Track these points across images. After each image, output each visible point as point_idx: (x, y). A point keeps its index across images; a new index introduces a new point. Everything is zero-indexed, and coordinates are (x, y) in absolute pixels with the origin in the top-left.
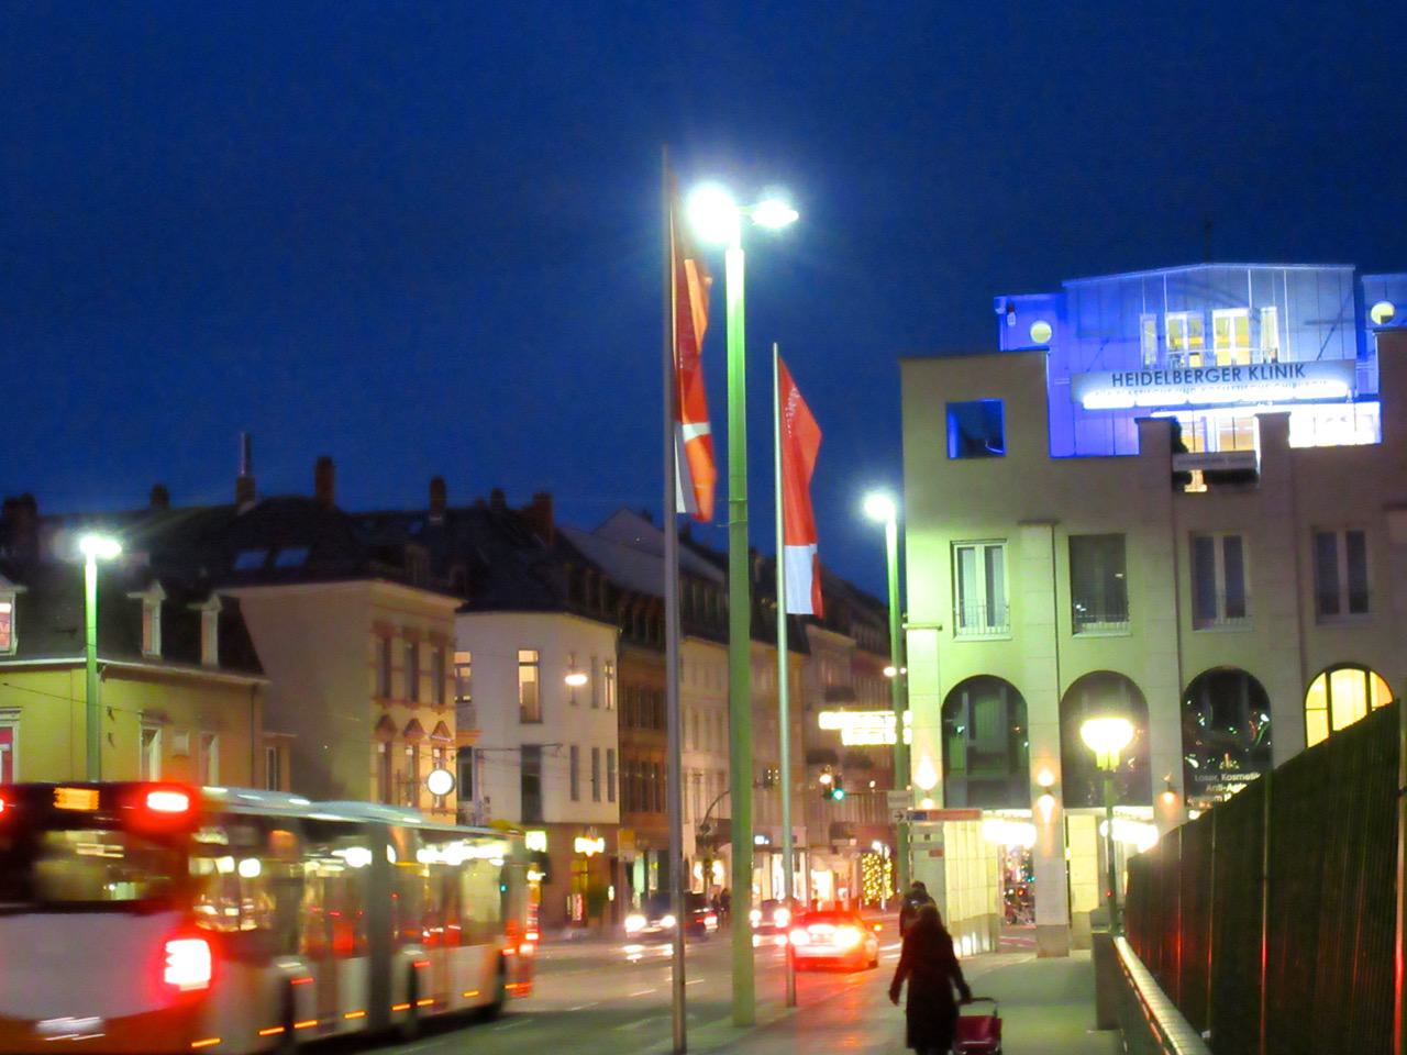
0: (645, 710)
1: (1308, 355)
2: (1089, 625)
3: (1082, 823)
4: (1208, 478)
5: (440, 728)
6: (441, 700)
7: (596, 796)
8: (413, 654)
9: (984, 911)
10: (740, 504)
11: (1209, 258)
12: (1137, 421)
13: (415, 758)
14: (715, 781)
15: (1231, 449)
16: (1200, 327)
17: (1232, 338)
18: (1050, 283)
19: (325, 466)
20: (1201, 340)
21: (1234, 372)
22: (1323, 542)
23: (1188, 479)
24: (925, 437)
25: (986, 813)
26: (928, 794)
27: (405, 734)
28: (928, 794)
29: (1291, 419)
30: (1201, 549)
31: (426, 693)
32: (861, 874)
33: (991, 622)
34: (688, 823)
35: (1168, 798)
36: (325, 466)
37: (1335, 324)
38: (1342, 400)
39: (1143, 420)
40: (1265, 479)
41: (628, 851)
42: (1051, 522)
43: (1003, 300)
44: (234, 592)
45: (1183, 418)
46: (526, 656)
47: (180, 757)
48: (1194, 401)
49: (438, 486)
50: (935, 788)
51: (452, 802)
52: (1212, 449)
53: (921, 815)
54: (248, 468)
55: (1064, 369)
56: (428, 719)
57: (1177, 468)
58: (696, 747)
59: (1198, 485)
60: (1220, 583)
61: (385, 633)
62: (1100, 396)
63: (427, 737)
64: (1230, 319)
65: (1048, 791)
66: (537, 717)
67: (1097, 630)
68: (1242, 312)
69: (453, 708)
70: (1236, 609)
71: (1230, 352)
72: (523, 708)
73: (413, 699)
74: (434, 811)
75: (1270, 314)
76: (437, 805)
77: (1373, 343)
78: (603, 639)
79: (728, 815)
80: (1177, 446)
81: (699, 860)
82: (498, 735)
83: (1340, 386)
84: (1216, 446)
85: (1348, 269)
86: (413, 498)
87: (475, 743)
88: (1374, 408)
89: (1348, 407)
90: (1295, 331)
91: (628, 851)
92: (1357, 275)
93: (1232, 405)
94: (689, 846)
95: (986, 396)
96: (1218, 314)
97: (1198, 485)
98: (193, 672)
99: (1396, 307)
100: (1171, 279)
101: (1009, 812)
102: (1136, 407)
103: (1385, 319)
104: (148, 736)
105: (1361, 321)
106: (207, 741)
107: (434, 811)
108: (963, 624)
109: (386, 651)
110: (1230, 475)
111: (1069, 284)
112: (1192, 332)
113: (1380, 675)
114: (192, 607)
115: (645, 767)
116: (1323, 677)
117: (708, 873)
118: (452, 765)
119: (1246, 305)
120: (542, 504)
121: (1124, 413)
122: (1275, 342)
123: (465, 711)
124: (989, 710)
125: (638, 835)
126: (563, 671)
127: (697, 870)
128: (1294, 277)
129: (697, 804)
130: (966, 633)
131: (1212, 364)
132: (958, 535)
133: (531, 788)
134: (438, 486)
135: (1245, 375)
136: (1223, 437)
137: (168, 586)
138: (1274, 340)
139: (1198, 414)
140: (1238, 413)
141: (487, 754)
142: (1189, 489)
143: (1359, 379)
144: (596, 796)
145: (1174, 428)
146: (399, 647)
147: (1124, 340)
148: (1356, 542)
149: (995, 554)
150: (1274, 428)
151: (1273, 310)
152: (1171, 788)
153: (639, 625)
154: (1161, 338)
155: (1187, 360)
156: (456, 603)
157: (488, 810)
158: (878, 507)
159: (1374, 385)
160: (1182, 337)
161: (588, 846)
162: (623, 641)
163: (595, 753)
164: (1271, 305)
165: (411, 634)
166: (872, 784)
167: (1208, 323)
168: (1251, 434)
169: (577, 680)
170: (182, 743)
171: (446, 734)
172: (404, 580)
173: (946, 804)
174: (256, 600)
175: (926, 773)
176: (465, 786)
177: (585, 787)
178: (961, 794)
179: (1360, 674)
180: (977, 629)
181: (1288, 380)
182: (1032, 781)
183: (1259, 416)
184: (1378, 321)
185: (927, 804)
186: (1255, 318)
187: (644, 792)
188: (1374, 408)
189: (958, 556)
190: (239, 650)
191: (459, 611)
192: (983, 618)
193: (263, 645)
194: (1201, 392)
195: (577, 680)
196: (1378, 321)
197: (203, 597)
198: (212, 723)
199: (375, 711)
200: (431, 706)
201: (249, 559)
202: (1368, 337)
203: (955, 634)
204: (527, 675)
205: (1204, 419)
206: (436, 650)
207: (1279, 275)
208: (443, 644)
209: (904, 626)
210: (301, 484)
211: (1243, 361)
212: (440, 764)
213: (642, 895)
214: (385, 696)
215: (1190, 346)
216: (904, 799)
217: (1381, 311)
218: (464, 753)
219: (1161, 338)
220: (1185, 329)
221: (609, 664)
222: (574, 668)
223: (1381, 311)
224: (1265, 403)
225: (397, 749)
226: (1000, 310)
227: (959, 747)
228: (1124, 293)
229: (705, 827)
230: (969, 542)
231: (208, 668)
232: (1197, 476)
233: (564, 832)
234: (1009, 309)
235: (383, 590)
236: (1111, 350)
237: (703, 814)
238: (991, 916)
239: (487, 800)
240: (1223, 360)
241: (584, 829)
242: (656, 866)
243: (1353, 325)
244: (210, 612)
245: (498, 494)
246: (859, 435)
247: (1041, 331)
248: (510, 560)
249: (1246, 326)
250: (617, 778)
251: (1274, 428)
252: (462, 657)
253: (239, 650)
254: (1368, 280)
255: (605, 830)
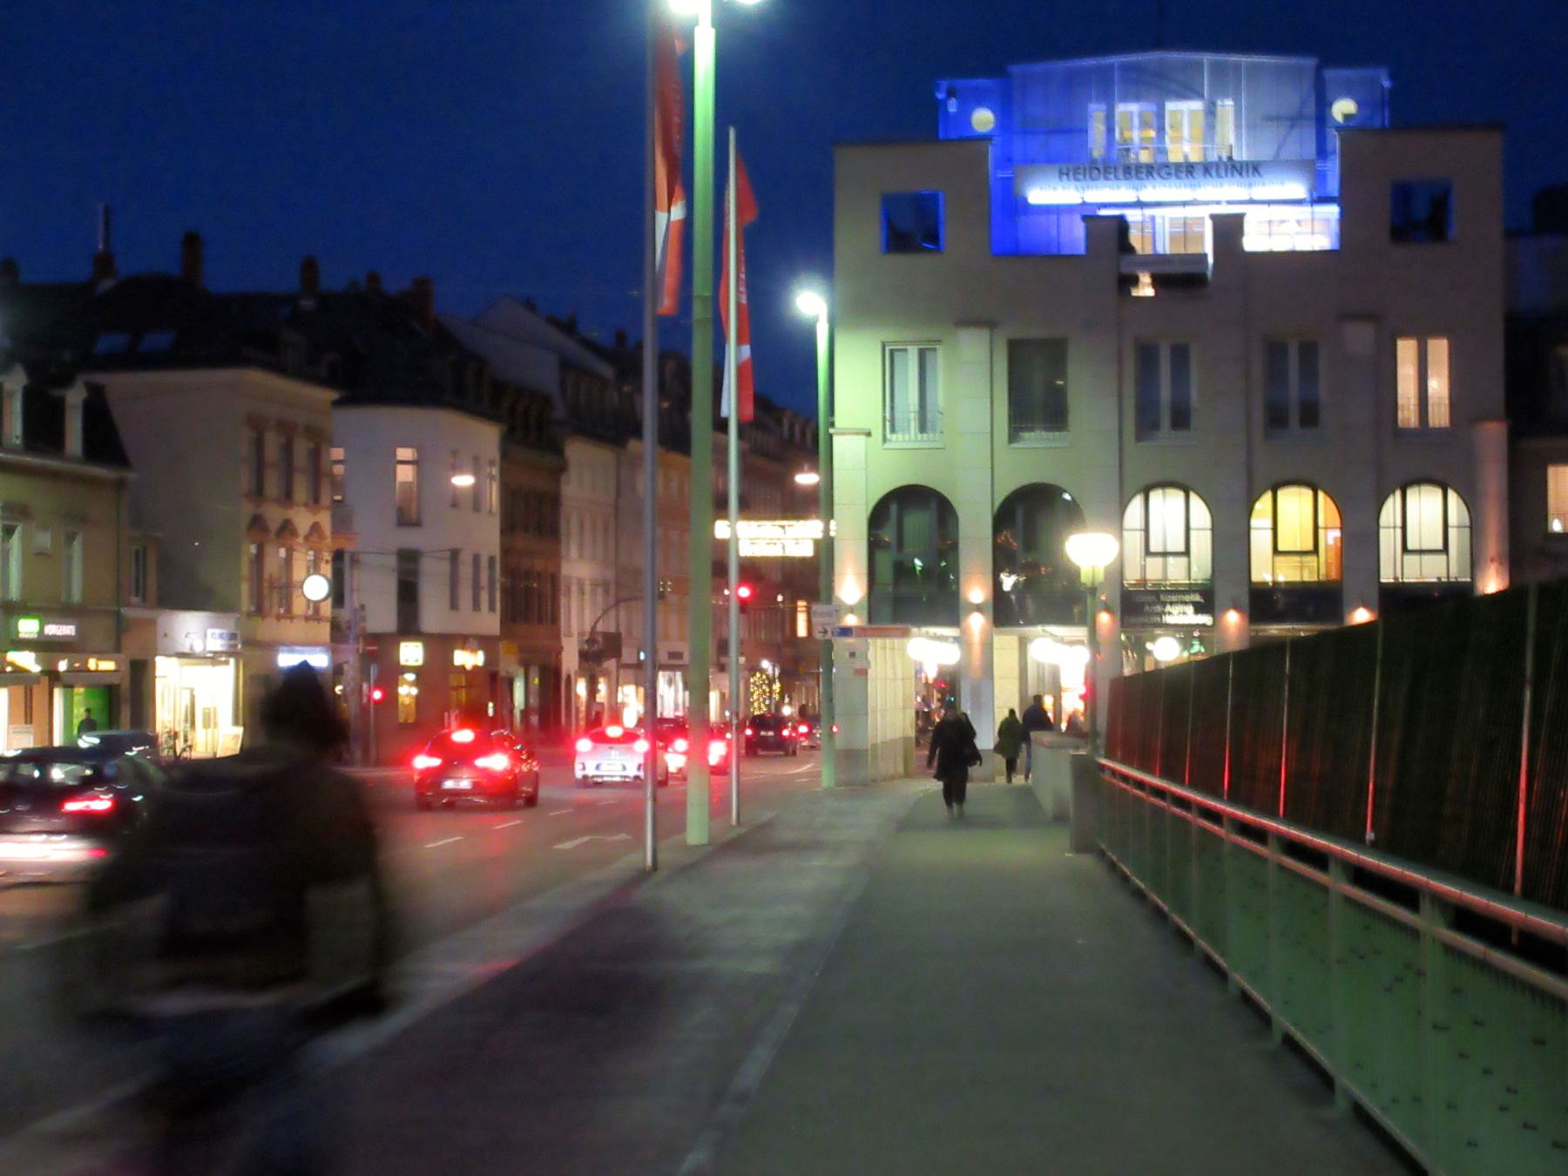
0: (531, 515)
1: (1265, 152)
2: (1026, 435)
3: (1006, 643)
4: (1157, 281)
5: (316, 528)
6: (316, 500)
7: (476, 606)
8: (288, 449)
9: (899, 734)
10: (704, 299)
11: (1159, 44)
12: (1085, 218)
13: (289, 561)
14: (600, 590)
15: (1182, 251)
16: (1153, 120)
17: (1186, 133)
18: (995, 69)
19: (192, 242)
20: (1152, 133)
21: (1187, 170)
22: (1275, 352)
23: (1135, 281)
24: (857, 231)
25: (915, 630)
26: (852, 610)
27: (307, 538)
28: (852, 610)
29: (1246, 219)
30: (1147, 357)
31: (301, 492)
32: (749, 694)
33: (923, 428)
34: (570, 635)
35: (1104, 618)
36: (192, 242)
37: (1294, 120)
38: (1299, 202)
39: (1090, 217)
40: (1219, 282)
41: (509, 664)
42: (990, 324)
43: (944, 84)
44: (100, 378)
45: (1133, 216)
46: (404, 453)
47: (41, 554)
48: (1200, 198)
49: (310, 268)
50: (860, 603)
51: (327, 609)
52: (1160, 250)
53: (846, 632)
54: (107, 240)
55: (1007, 161)
56: (303, 520)
57: (1125, 270)
58: (581, 556)
59: (1145, 289)
60: (1165, 394)
61: (257, 425)
62: (1044, 192)
63: (301, 540)
64: (1184, 111)
65: (979, 608)
66: (414, 515)
67: (1035, 439)
68: (1196, 105)
69: (327, 508)
70: (1181, 419)
71: (1184, 148)
72: (400, 510)
73: (287, 498)
74: (307, 618)
75: (1227, 106)
76: (311, 612)
77: (1335, 142)
78: (487, 436)
79: (612, 629)
80: (1125, 247)
81: (581, 676)
82: (377, 538)
83: (1297, 188)
84: (1165, 247)
85: (1310, 62)
86: (288, 281)
87: (349, 547)
88: (1333, 210)
89: (1305, 211)
90: (1252, 127)
91: (509, 664)
92: (1319, 69)
93: (1184, 204)
94: (570, 660)
95: (925, 188)
96: (1171, 106)
97: (1145, 289)
98: (52, 463)
99: (1360, 104)
100: (1126, 68)
101: (933, 630)
102: (1084, 204)
103: (1347, 117)
104: (9, 531)
105: (1322, 117)
106: (70, 538)
107: (307, 618)
108: (893, 430)
109: (259, 444)
110: (1180, 278)
111: (1016, 69)
112: (1144, 125)
113: (1326, 493)
114: (57, 392)
115: (528, 575)
116: (1268, 497)
117: (592, 691)
118: (327, 569)
119: (1200, 96)
120: (422, 288)
121: (1069, 209)
122: (1231, 138)
123: (342, 521)
124: (918, 522)
125: (522, 650)
126: (457, 472)
127: (581, 688)
128: (1253, 68)
129: (579, 617)
130: (897, 440)
131: (1161, 159)
132: (889, 335)
133: (408, 594)
134: (310, 268)
135: (1198, 173)
136: (1173, 237)
137: (31, 370)
138: (1231, 138)
139: (1148, 212)
140: (1191, 212)
141: (363, 558)
142: (1136, 293)
143: (1318, 179)
144: (476, 606)
145: (1122, 225)
146: (273, 443)
147: (1069, 131)
148: (1309, 352)
149: (929, 355)
150: (1228, 229)
151: (1229, 103)
152: (1108, 609)
153: (533, 432)
154: (1110, 130)
155: (1137, 154)
156: (331, 395)
157: (363, 619)
158: (809, 302)
159: (1333, 186)
160: (1131, 129)
161: (468, 659)
162: (507, 440)
163: (476, 559)
164: (1227, 96)
165: (287, 430)
166: (780, 598)
167: (1160, 115)
168: (1201, 236)
169: (464, 481)
170: (44, 540)
171: (322, 537)
172: (280, 369)
173: (870, 619)
174: (118, 384)
175: (850, 587)
176: (338, 594)
177: (466, 593)
178: (886, 610)
179: (1307, 494)
180: (908, 437)
181: (1245, 180)
182: (962, 597)
183: (1214, 217)
184: (1339, 118)
185: (851, 620)
186: (1211, 112)
187: (528, 602)
188: (1333, 210)
189: (890, 358)
190: (104, 442)
191: (337, 404)
192: (914, 425)
193: (129, 435)
194: (1152, 191)
195: (464, 481)
196: (1339, 118)
197: (66, 381)
198: (74, 521)
199: (247, 509)
200: (306, 505)
201: (108, 342)
202: (1329, 136)
203: (885, 439)
204: (405, 474)
205: (1153, 219)
206: (311, 445)
207: (1237, 67)
208: (319, 440)
209: (831, 431)
210: (164, 261)
211: (1194, 157)
212: (315, 568)
213: (522, 712)
214: (258, 493)
215: (1142, 139)
216: (830, 614)
217: (1343, 108)
218: (338, 556)
219: (1110, 130)
220: (1136, 121)
221: (492, 463)
222: (457, 469)
223: (1343, 108)
224: (1218, 203)
225: (269, 549)
226: (940, 96)
227: (885, 561)
228: (1071, 82)
229: (592, 641)
230: (905, 342)
231: (72, 459)
232: (1145, 279)
233: (441, 645)
234: (951, 93)
235: (256, 377)
236: (1058, 143)
237: (588, 628)
238: (906, 739)
239: (363, 607)
240: (1175, 157)
241: (464, 641)
242: (537, 681)
243: (1313, 122)
244: (75, 397)
245: (373, 278)
246: (790, 226)
247: (983, 119)
248: (388, 352)
249: (1201, 119)
250: (498, 586)
251: (1228, 229)
252: (338, 453)
253: (104, 442)
254: (1330, 74)
255: (484, 642)
